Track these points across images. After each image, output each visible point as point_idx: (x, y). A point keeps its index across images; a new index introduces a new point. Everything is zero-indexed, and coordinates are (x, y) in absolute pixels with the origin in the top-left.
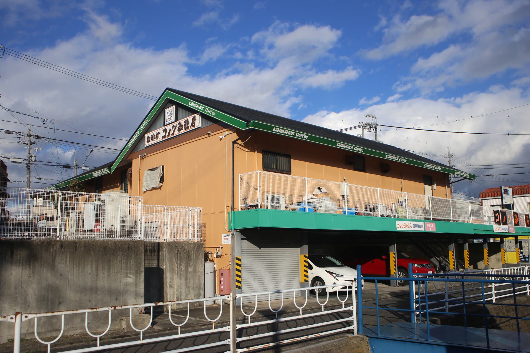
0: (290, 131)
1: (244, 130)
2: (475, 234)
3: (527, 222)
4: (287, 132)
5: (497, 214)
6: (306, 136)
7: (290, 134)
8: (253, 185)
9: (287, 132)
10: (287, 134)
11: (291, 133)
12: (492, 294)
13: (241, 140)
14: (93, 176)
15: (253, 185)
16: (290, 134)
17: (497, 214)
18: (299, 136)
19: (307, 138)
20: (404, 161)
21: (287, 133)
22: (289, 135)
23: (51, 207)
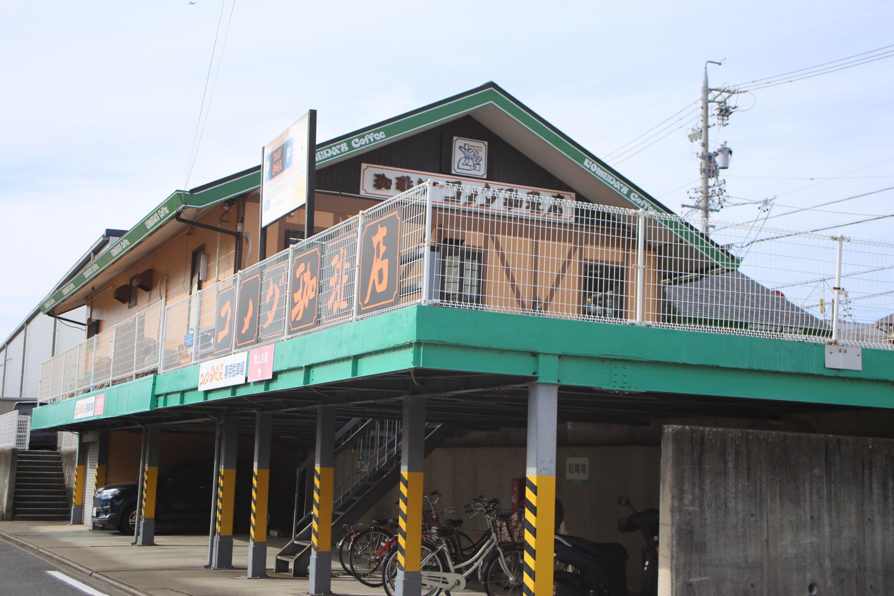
0: (333, 148)
1: (491, 102)
2: (661, 455)
3: (374, 276)
4: (327, 152)
5: (378, 291)
6: (377, 134)
7: (339, 152)
8: (680, 304)
9: (327, 152)
10: (332, 156)
11: (340, 150)
12: (690, 247)
13: (376, 291)
14: (582, 163)
15: (680, 304)
16: (339, 152)
17: (378, 291)
18: (363, 143)
19: (167, 212)
20: (357, 139)
21: (329, 155)
22: (337, 155)
23: (817, 281)
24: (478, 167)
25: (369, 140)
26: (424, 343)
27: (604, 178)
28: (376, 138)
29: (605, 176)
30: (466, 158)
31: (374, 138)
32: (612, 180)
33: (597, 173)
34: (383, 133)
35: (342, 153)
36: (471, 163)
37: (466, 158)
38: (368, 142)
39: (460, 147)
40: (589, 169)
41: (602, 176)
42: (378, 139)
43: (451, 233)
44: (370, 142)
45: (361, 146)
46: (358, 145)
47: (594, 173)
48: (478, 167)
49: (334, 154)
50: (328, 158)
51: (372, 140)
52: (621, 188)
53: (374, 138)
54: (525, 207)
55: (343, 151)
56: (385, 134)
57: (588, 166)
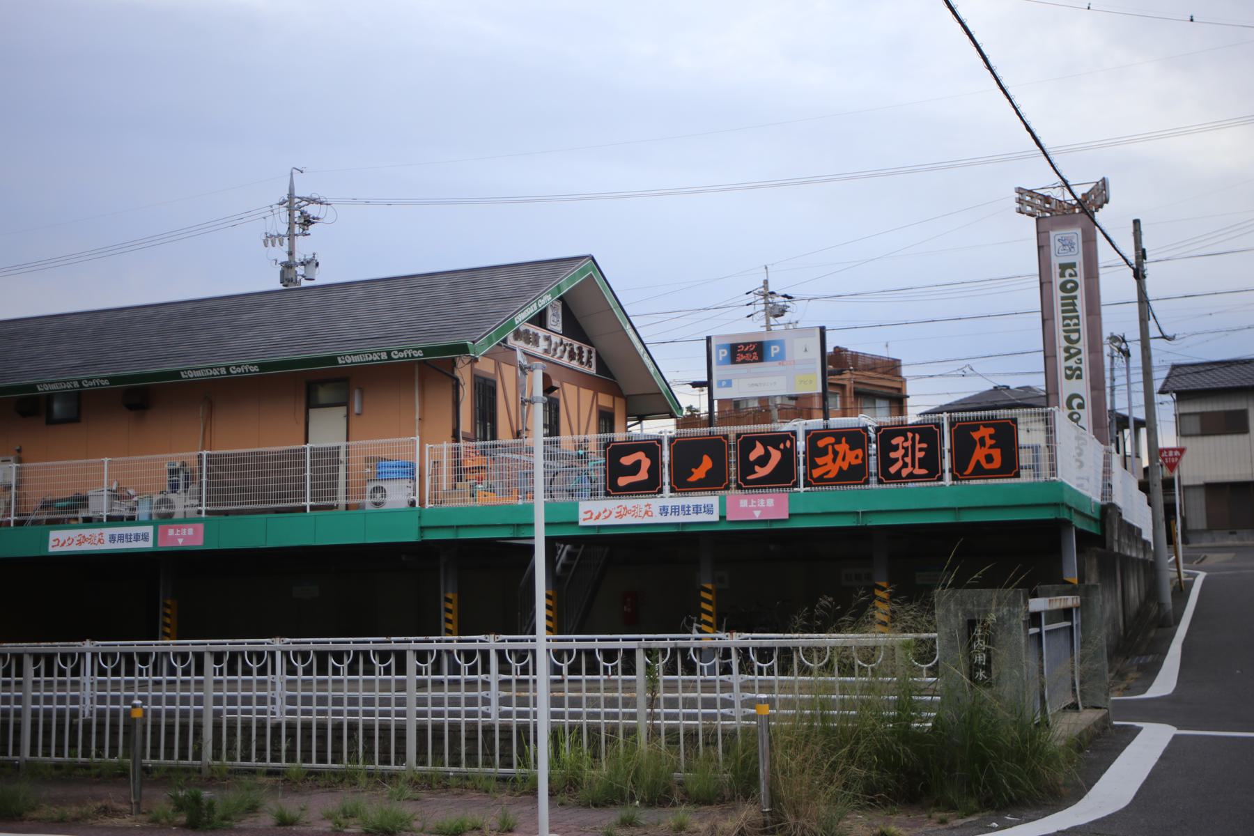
6: (416, 352)
10: (213, 375)
14: (181, 378)
21: (370, 359)
22: (377, 361)
24: (1072, 250)
25: (408, 355)
26: (1053, 465)
27: (362, 360)
28: (414, 355)
29: (361, 358)
30: (1064, 245)
31: (412, 354)
32: (369, 356)
33: (354, 361)
34: (257, 367)
35: (381, 360)
36: (1067, 248)
37: (1064, 245)
38: (406, 356)
39: (1059, 240)
40: (346, 363)
41: (359, 361)
42: (252, 370)
43: (566, 446)
44: (245, 373)
45: (238, 373)
46: (235, 372)
47: (194, 377)
48: (1072, 250)
49: (375, 359)
50: (209, 376)
51: (410, 356)
52: (380, 357)
53: (412, 354)
54: (528, 328)
55: (382, 358)
56: (423, 352)
57: (344, 362)
